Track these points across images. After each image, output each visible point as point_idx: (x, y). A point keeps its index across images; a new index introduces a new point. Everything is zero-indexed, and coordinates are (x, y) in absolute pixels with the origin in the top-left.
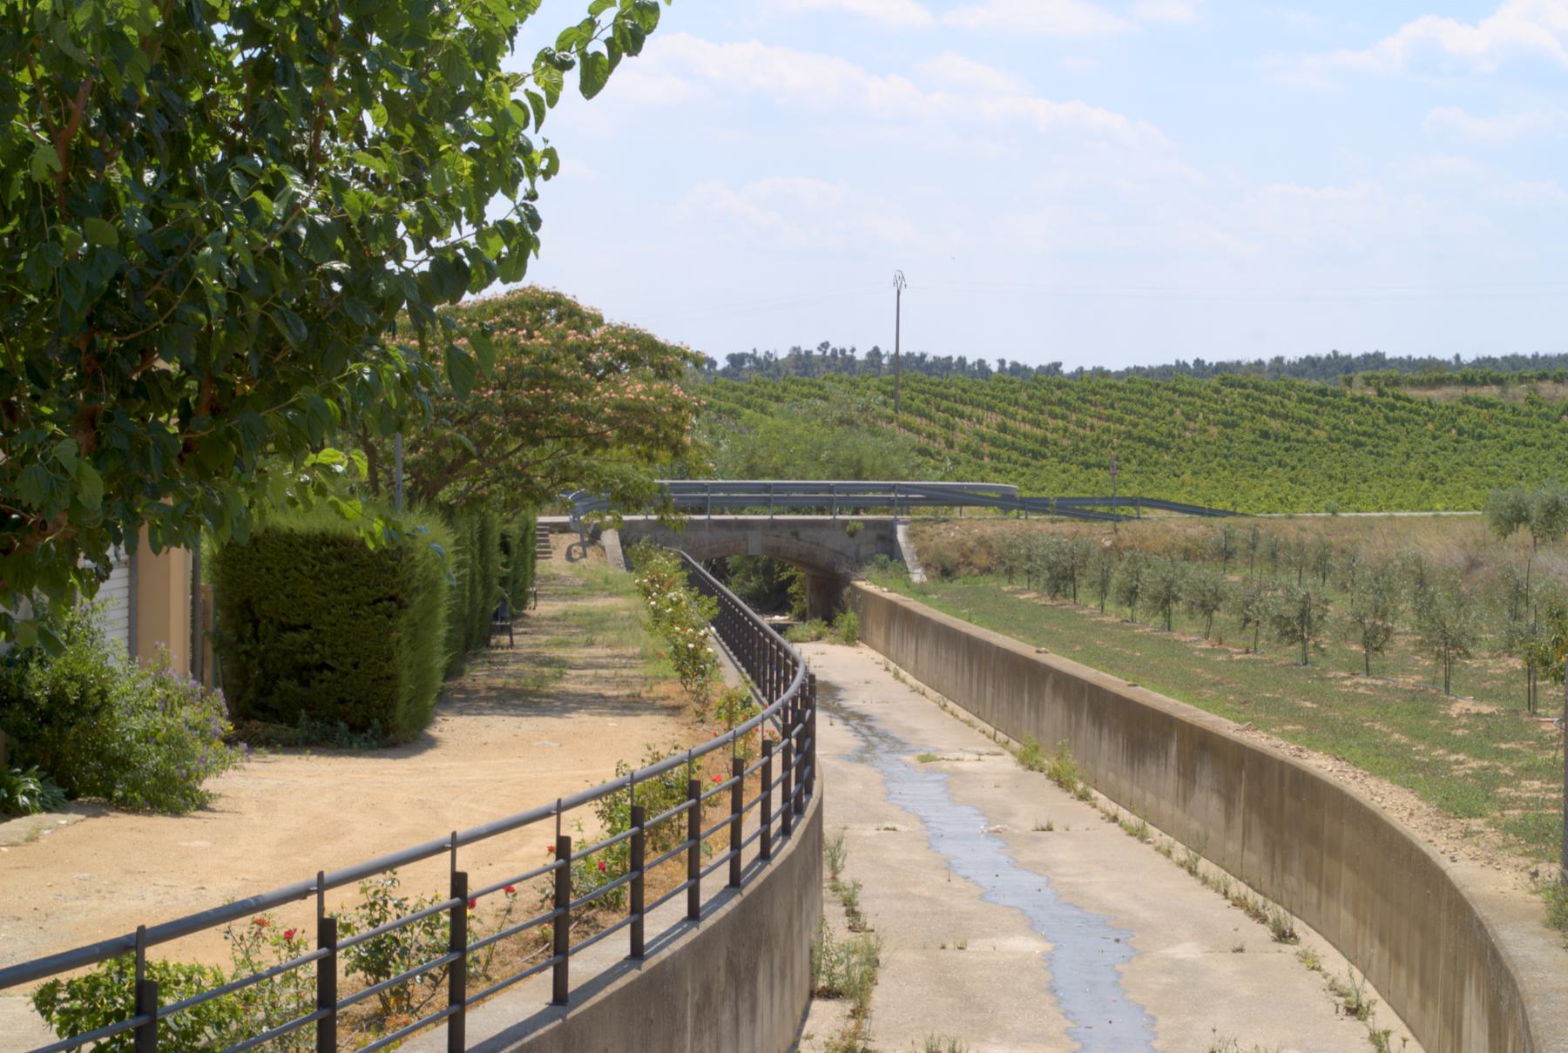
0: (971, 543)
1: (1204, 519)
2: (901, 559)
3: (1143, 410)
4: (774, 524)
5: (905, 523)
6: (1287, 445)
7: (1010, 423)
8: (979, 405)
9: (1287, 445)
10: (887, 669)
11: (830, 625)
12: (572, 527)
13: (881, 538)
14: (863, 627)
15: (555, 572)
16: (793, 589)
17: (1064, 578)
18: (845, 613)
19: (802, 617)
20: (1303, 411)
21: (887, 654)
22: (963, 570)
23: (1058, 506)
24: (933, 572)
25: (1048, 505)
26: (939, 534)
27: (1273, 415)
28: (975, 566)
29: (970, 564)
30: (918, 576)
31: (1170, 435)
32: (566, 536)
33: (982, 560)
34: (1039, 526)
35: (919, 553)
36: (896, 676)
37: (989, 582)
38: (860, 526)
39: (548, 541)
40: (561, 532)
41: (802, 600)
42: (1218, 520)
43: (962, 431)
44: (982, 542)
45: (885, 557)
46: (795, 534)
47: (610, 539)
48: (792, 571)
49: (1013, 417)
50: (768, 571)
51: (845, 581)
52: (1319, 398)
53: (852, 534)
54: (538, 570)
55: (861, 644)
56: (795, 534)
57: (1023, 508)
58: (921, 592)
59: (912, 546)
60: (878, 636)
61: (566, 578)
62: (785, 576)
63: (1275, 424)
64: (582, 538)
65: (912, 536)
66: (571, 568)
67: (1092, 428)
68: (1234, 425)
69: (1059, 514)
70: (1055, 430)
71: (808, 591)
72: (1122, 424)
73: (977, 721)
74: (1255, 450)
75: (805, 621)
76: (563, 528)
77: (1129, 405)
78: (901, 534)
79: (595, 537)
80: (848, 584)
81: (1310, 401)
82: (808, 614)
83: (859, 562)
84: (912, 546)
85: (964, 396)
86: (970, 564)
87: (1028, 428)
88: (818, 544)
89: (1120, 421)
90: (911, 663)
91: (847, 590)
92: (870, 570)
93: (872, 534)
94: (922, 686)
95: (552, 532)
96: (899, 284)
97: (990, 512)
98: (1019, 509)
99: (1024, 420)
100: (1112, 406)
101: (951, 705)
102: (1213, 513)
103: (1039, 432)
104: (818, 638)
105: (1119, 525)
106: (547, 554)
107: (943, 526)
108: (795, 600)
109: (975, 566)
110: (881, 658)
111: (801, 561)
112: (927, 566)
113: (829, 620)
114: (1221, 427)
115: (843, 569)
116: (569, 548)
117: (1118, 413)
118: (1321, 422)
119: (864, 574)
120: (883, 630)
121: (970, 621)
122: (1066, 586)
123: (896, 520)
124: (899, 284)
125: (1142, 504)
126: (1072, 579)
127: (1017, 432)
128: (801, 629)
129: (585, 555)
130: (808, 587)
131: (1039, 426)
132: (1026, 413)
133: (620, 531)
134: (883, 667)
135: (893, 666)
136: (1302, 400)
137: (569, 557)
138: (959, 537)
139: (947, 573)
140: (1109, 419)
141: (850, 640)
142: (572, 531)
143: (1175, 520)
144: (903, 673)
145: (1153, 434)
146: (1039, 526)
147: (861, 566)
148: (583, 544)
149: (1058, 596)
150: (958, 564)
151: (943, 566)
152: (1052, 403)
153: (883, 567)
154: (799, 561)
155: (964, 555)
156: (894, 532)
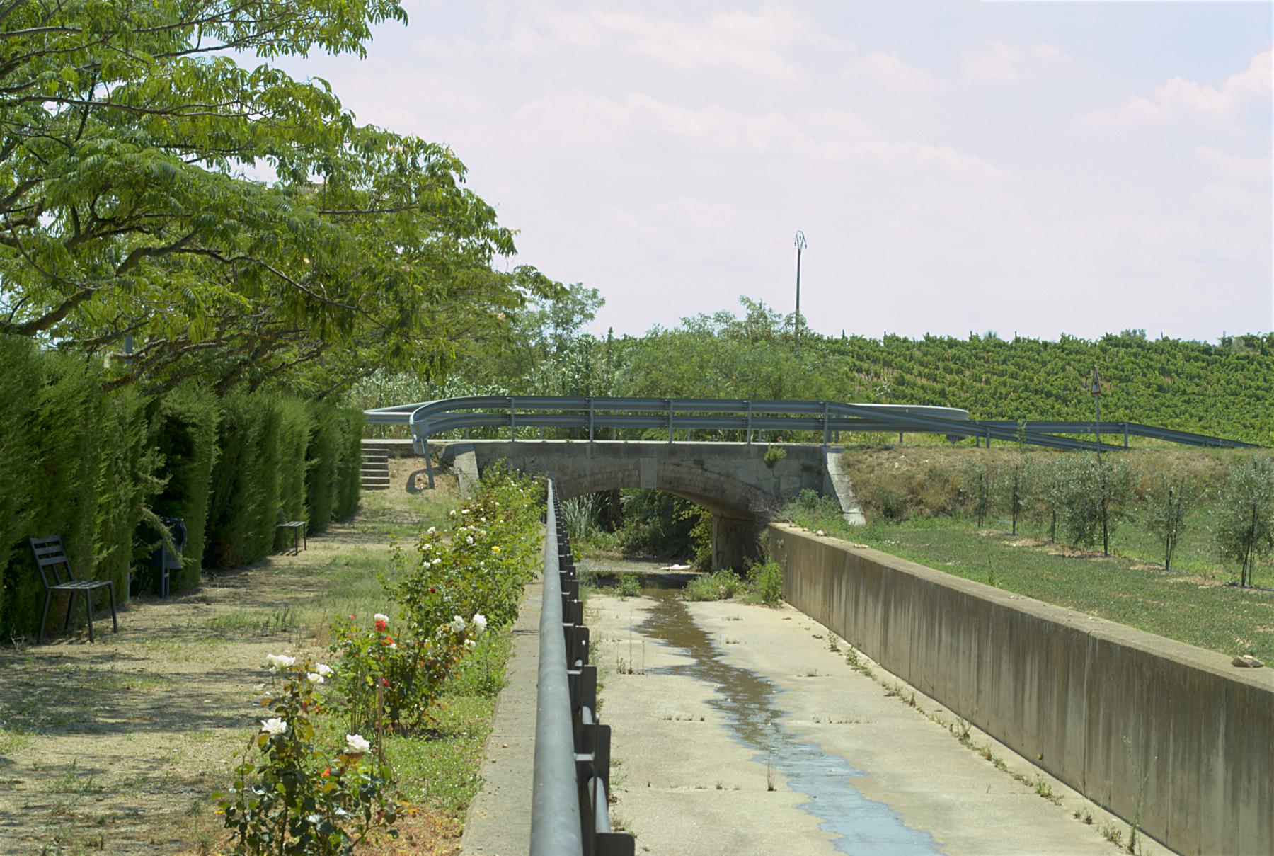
0: (921, 477)
1: (1208, 450)
2: (832, 495)
3: (1036, 366)
4: (673, 450)
5: (837, 451)
6: (1186, 398)
7: (908, 377)
8: (875, 361)
9: (1186, 398)
10: (834, 649)
11: (743, 578)
12: (416, 450)
13: (807, 469)
14: (789, 585)
15: (388, 505)
16: (696, 531)
17: (1092, 517)
18: (763, 563)
19: (707, 567)
20: (1191, 368)
21: (825, 620)
22: (911, 511)
23: (1028, 432)
24: (872, 512)
25: (1015, 431)
26: (880, 465)
27: (1163, 371)
28: (926, 505)
29: (920, 502)
30: (856, 518)
31: (1066, 388)
32: (409, 461)
33: (936, 497)
34: (1005, 456)
35: (854, 488)
36: (852, 661)
37: (943, 522)
38: (781, 453)
39: (385, 467)
40: (403, 456)
41: (707, 545)
42: (1226, 451)
43: (860, 384)
44: (933, 474)
45: (813, 492)
46: (700, 463)
47: (466, 463)
48: (696, 509)
49: (910, 371)
50: (666, 512)
51: (761, 522)
52: (1205, 356)
53: (771, 464)
54: (363, 502)
55: (785, 605)
56: (700, 463)
57: (984, 435)
58: (871, 535)
59: (847, 479)
60: (815, 596)
61: (401, 513)
62: (686, 515)
63: (1166, 381)
64: (428, 464)
65: (846, 466)
66: (410, 502)
67: (988, 382)
68: (1127, 380)
69: (1028, 442)
70: (952, 384)
71: (714, 535)
72: (1016, 379)
73: (1098, 813)
74: (1157, 402)
75: (711, 572)
76: (407, 452)
77: (1022, 362)
78: (832, 463)
79: (446, 461)
80: (766, 526)
81: (1196, 359)
82: (714, 564)
83: (779, 499)
84: (847, 479)
85: (861, 352)
86: (920, 502)
87: (925, 382)
88: (728, 476)
89: (1014, 376)
90: (874, 642)
91: (764, 534)
92: (793, 508)
93: (796, 464)
94: (908, 690)
95: (393, 457)
96: (800, 242)
97: (938, 440)
98: (978, 435)
99: (920, 374)
100: (1005, 362)
101: (977, 736)
102: (1213, 443)
103: (938, 386)
104: (729, 595)
105: (1103, 456)
106: (382, 484)
107: (885, 454)
108: (698, 546)
109: (926, 505)
110: (821, 629)
111: (707, 497)
112: (865, 505)
113: (742, 571)
114: (1115, 382)
115: (760, 507)
116: (413, 476)
117: (1012, 369)
118: (1214, 378)
119: (786, 515)
120: (820, 588)
121: (991, 582)
122: (1093, 528)
123: (825, 446)
124: (800, 242)
125: (1130, 432)
126: (1104, 517)
127: (915, 384)
128: (706, 583)
129: (431, 485)
130: (714, 530)
131: (935, 380)
132: (921, 369)
133: (479, 456)
134: (828, 644)
135: (843, 644)
136: (1188, 359)
137: (411, 487)
138: (905, 468)
139: (891, 513)
140: (1002, 374)
141: (770, 599)
142: (418, 456)
143: (1175, 454)
144: (862, 657)
145: (1049, 388)
146: (1005, 456)
147: (782, 503)
148: (430, 471)
149: (1081, 545)
150: (905, 502)
151: (886, 503)
152: (945, 359)
153: (810, 506)
154: (703, 497)
155: (912, 491)
156: (824, 462)
